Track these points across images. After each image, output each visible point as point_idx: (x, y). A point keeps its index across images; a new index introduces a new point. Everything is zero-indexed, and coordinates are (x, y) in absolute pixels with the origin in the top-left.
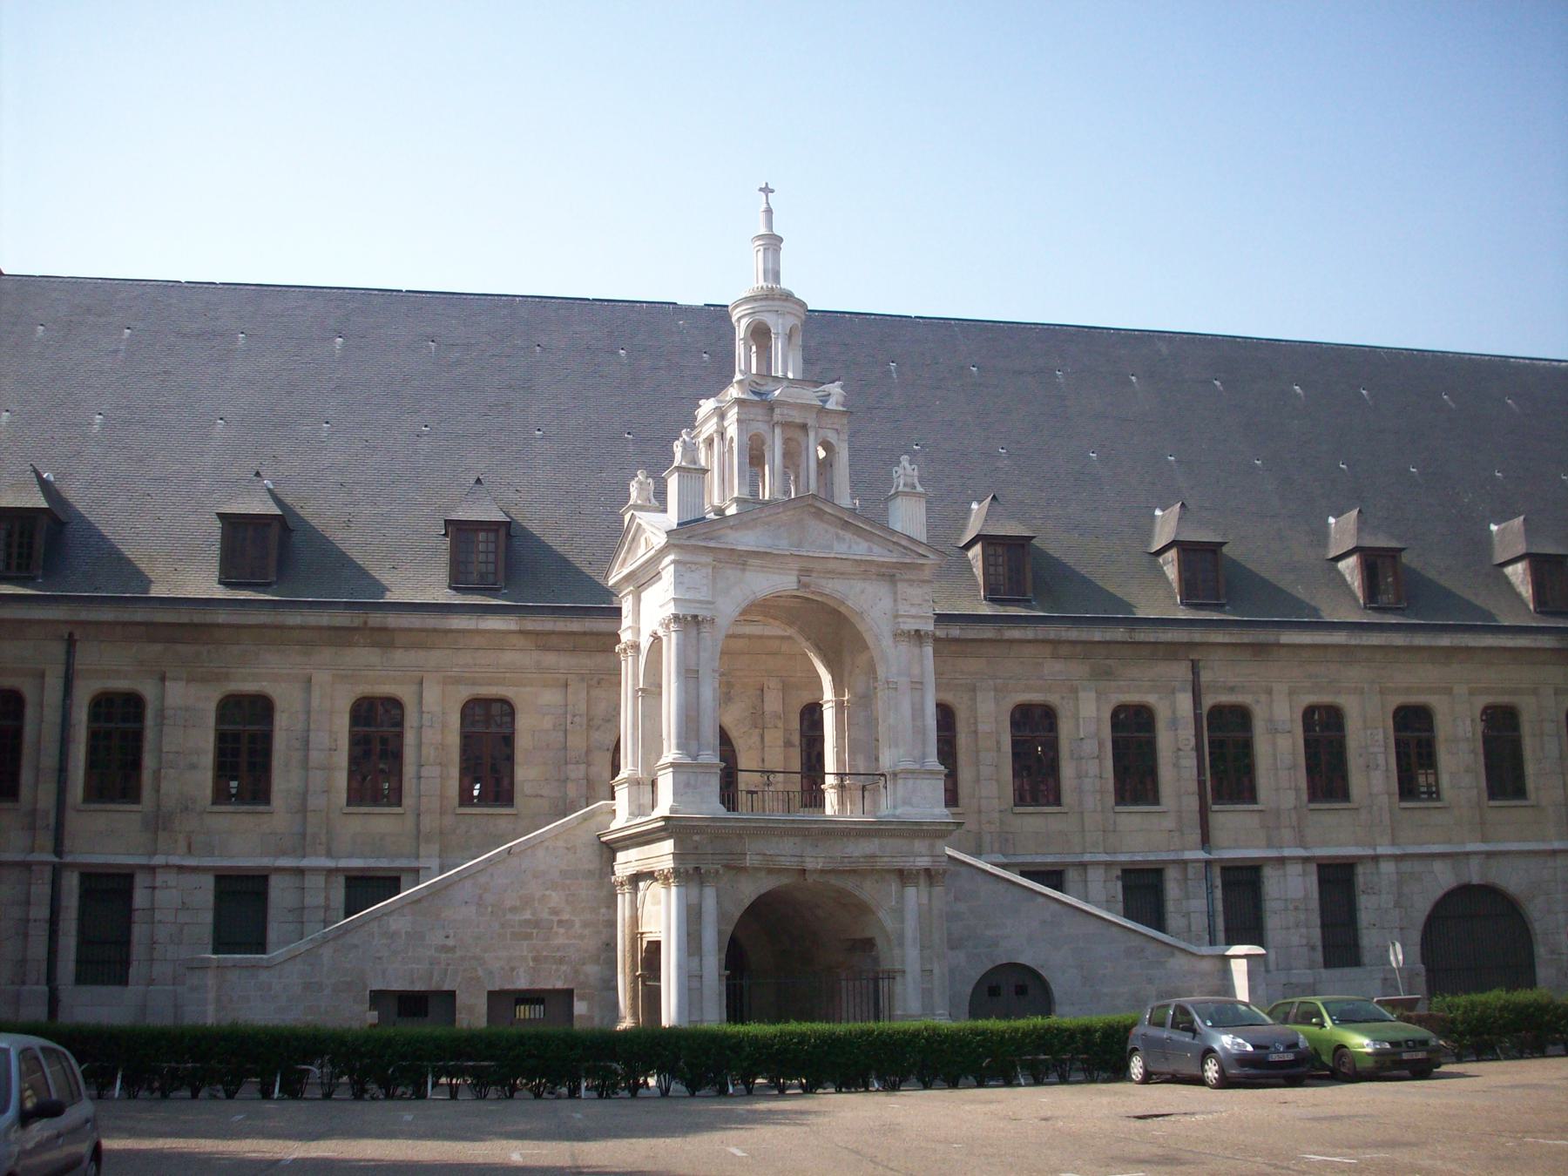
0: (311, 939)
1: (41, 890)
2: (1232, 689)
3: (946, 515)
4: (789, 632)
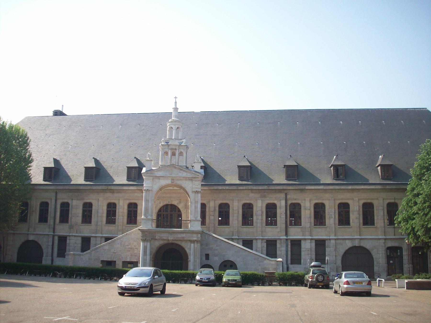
1: (51, 239)
2: (295, 199)
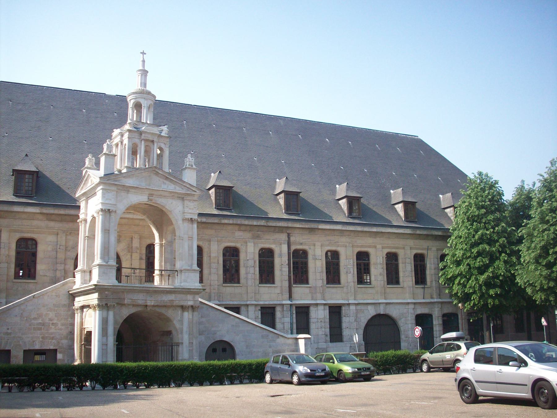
2: (301, 244)
3: (203, 177)
4: (144, 217)
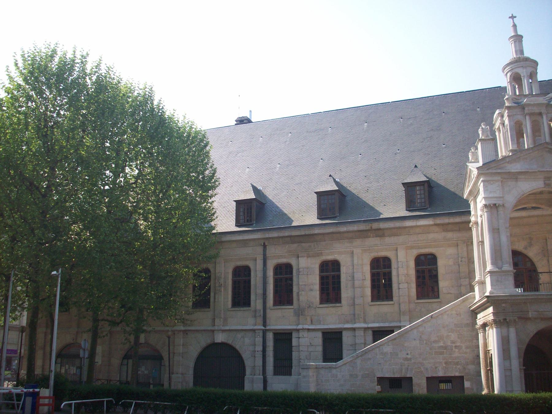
0: (352, 356)
1: (259, 340)
